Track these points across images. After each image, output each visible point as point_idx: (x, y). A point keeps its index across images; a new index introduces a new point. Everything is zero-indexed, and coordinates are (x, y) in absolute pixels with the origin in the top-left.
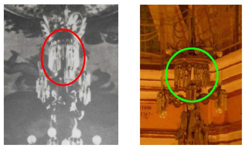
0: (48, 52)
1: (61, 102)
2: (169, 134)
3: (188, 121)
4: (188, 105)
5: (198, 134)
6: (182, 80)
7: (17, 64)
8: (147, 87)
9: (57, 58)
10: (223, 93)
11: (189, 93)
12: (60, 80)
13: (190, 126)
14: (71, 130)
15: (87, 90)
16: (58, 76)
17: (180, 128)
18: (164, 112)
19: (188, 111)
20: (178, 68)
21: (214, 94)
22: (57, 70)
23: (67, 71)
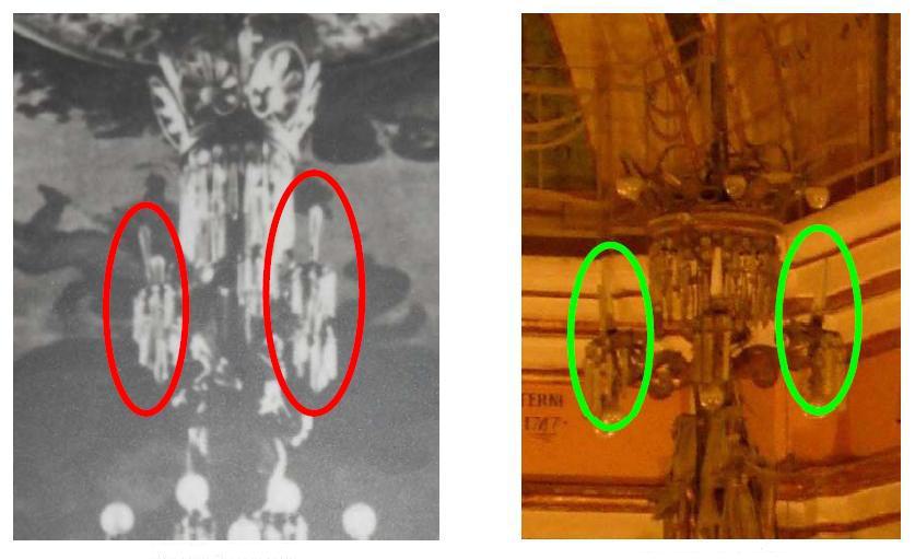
0: (177, 191)
1: (228, 380)
2: (632, 497)
3: (701, 451)
4: (700, 388)
5: (737, 495)
6: (679, 297)
7: (64, 236)
8: (548, 321)
9: (212, 214)
10: (830, 345)
11: (702, 342)
12: (221, 298)
13: (707, 467)
14: (263, 482)
15: (323, 335)
16: (216, 282)
17: (672, 474)
18: (609, 416)
19: (701, 412)
20: (664, 249)
21: (799, 347)
22: (209, 258)
23: (248, 262)
